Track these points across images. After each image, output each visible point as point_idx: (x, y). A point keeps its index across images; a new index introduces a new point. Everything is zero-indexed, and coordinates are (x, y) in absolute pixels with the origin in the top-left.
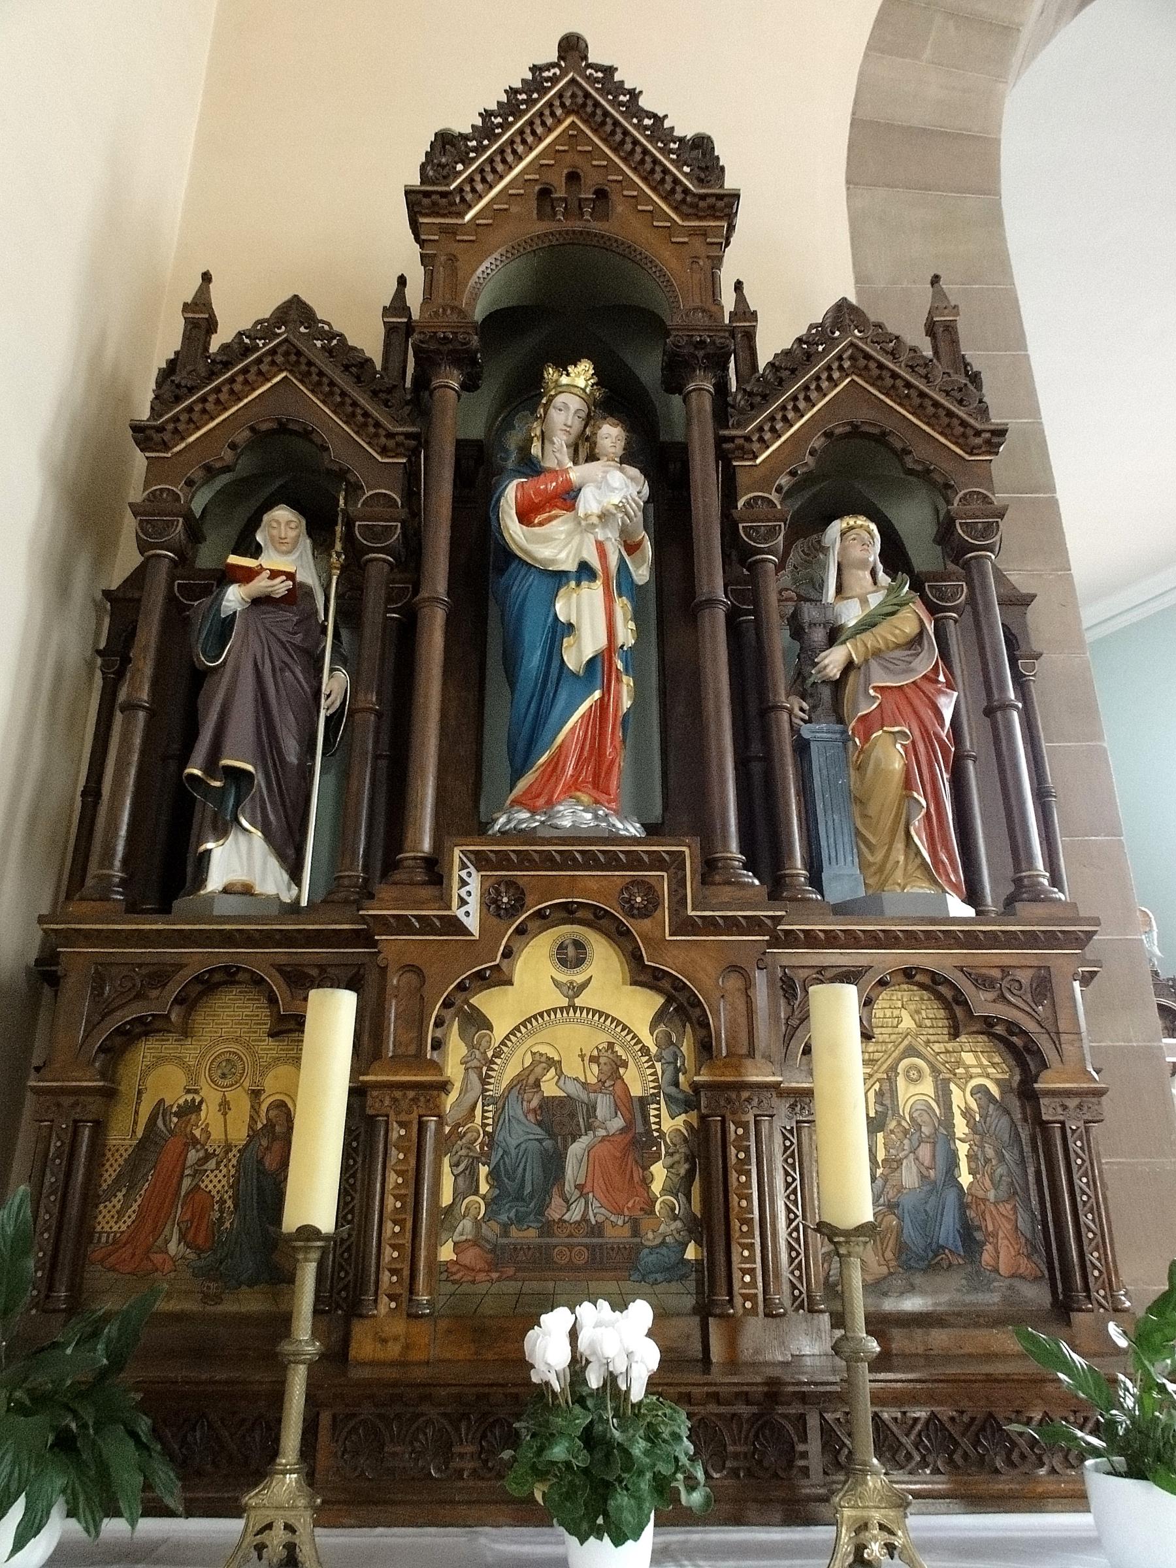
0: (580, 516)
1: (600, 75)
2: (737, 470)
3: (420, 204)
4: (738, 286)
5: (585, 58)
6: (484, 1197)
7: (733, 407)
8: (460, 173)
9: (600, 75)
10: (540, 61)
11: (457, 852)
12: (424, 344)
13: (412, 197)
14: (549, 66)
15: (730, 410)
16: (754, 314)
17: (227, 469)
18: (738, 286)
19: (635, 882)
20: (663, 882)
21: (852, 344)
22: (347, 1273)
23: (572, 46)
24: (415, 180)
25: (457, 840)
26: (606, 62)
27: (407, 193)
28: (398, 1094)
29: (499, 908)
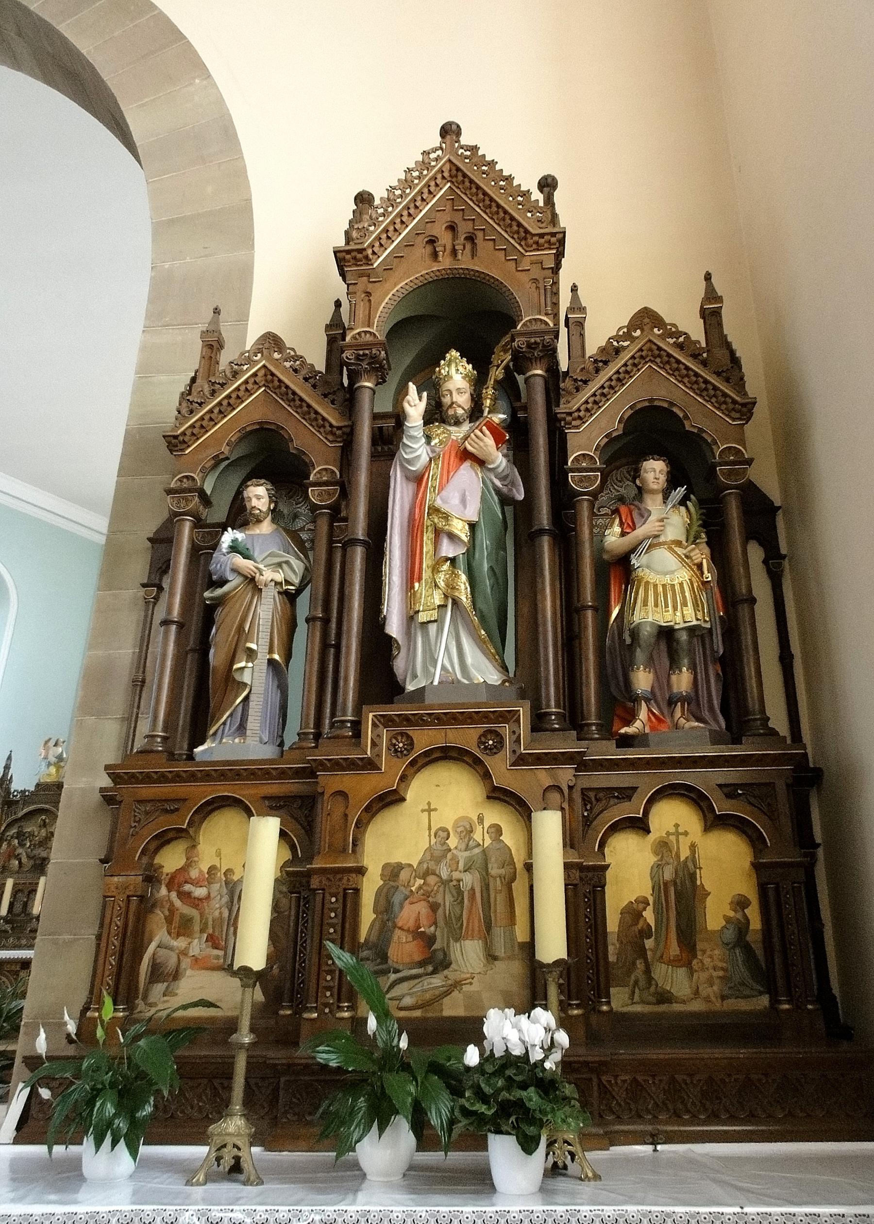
0: (449, 484)
1: (468, 153)
2: (568, 437)
3: (344, 259)
4: (574, 289)
5: (458, 141)
6: (392, 1018)
7: (563, 390)
8: (372, 232)
9: (468, 153)
10: (427, 148)
11: (371, 715)
12: (347, 366)
13: (338, 254)
14: (435, 150)
15: (562, 392)
16: (585, 308)
17: (227, 458)
18: (574, 289)
19: (490, 731)
20: (506, 730)
21: (650, 341)
22: (304, 955)
23: (449, 131)
24: (341, 242)
25: (370, 707)
26: (472, 143)
27: (335, 253)
28: (331, 876)
29: (396, 751)
